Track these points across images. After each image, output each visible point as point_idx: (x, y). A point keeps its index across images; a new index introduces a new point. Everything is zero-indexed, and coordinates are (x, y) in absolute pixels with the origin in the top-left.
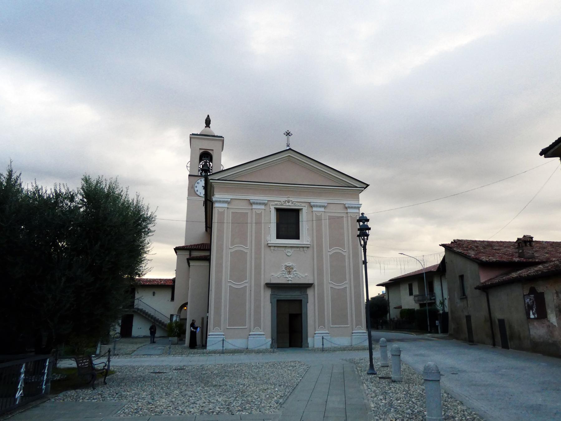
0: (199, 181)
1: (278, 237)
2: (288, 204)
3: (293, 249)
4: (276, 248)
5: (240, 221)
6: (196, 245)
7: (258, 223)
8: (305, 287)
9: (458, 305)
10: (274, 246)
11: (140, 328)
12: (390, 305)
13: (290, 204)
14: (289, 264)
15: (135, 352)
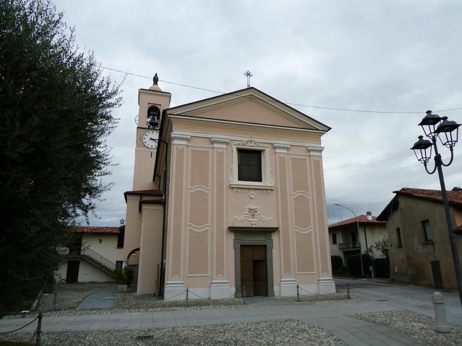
0: (147, 133)
1: (240, 179)
2: (250, 144)
5: (200, 158)
6: (147, 191)
8: (269, 232)
9: (419, 251)
10: (237, 188)
11: (85, 274)
13: (252, 144)
14: (252, 208)
15: (80, 305)
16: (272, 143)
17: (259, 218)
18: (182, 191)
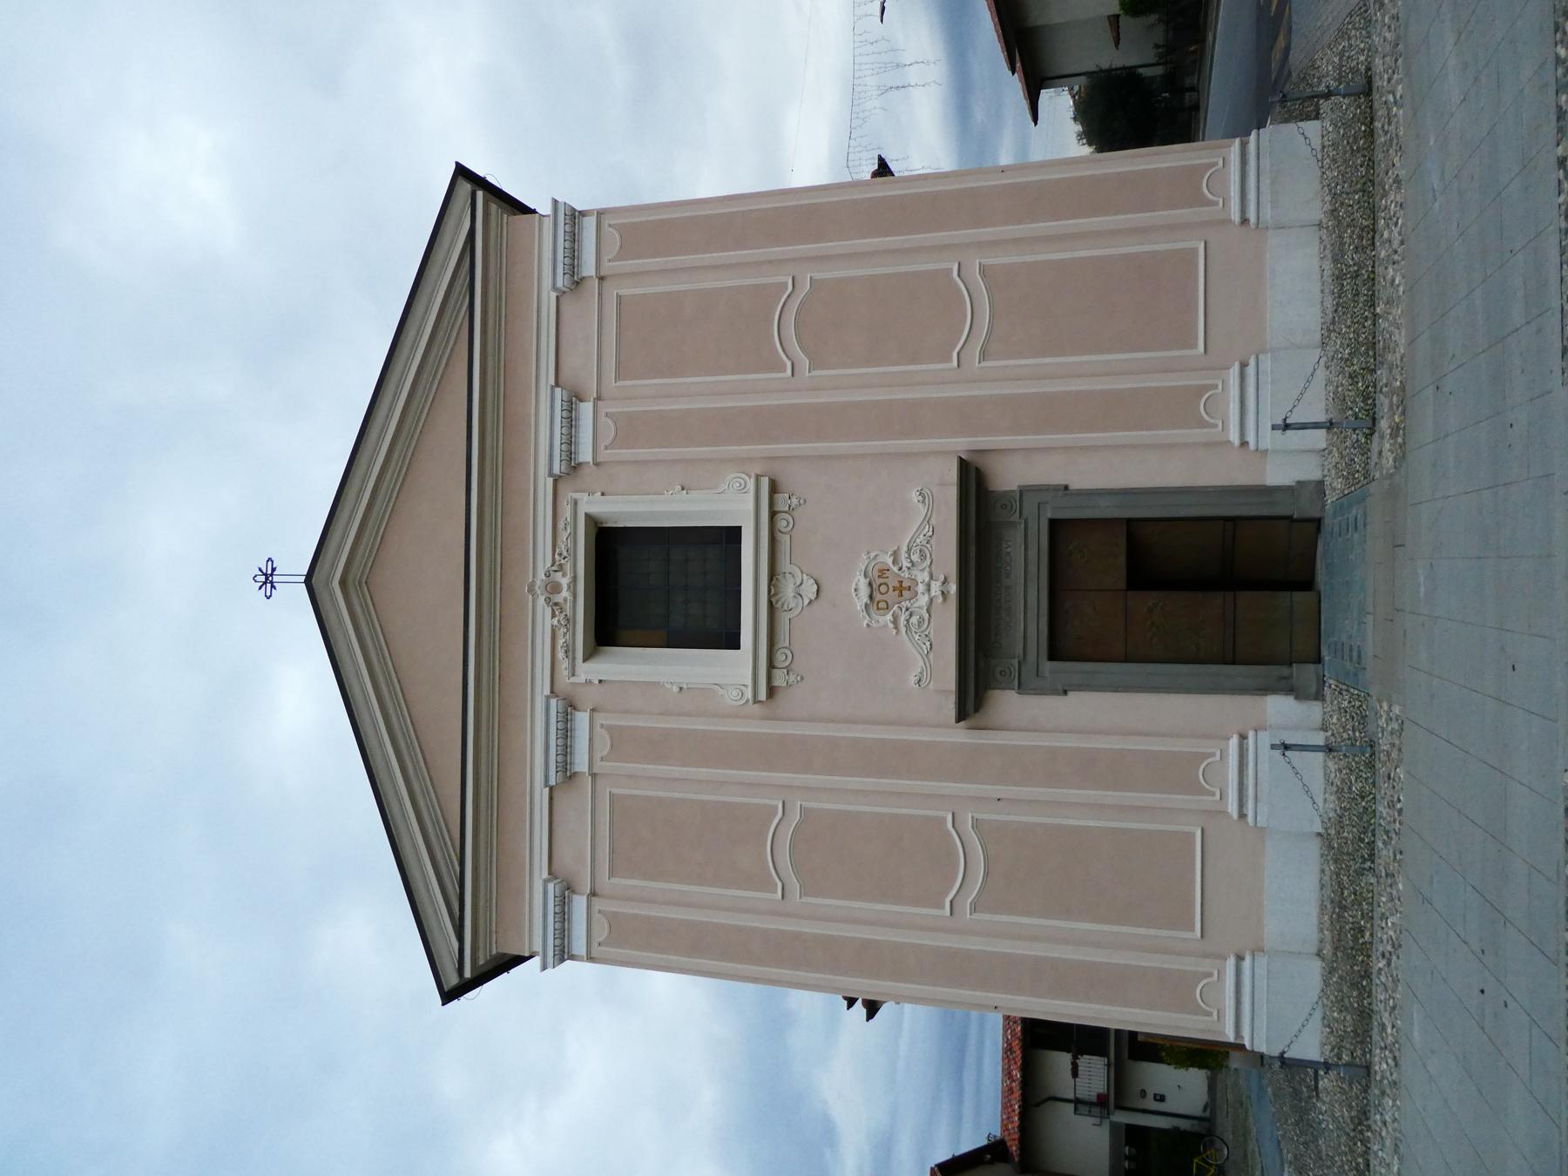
1: (733, 643)
2: (565, 593)
3: (785, 565)
4: (780, 658)
7: (656, 746)
8: (979, 503)
10: (771, 665)
12: (1105, 66)
13: (565, 582)
16: (550, 481)
17: (915, 558)
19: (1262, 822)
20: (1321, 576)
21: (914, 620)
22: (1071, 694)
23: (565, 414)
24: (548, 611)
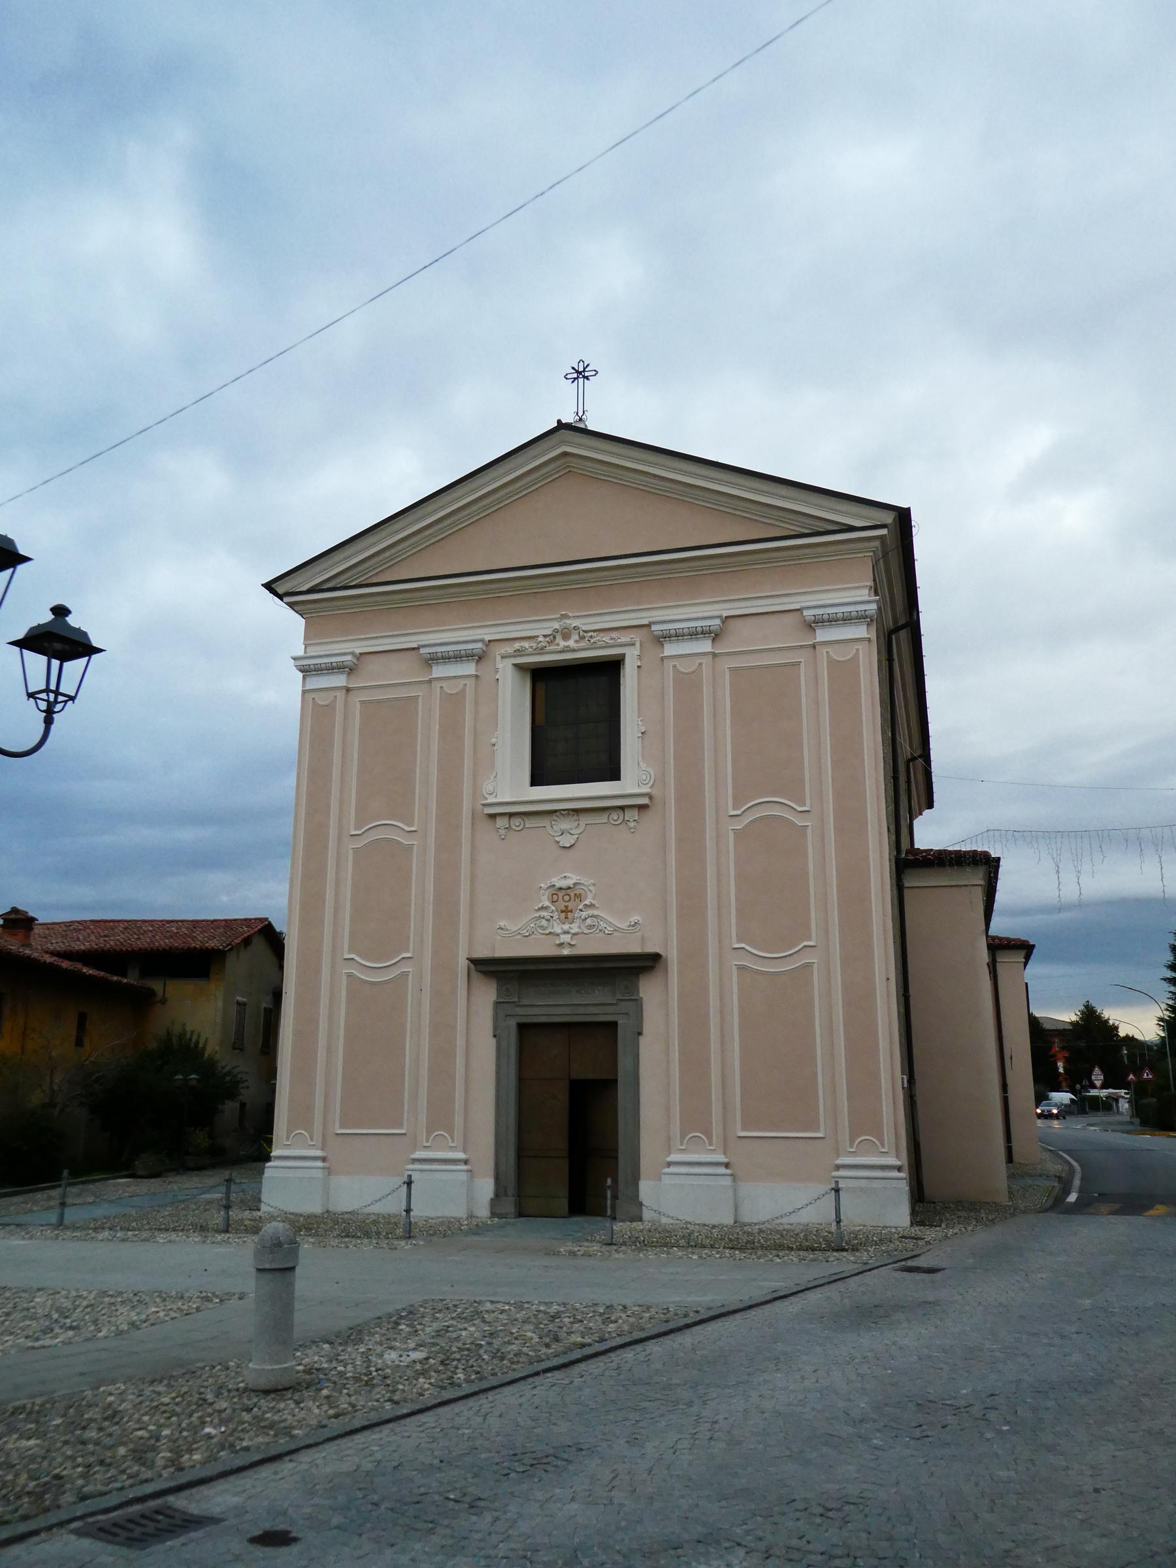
1: (537, 779)
2: (563, 644)
4: (516, 821)
7: (451, 729)
10: (511, 815)
13: (571, 643)
16: (646, 622)
17: (589, 921)
18: (326, 848)
19: (666, 1180)
20: (575, 1219)
21: (544, 923)
22: (493, 1041)
23: (699, 629)
24: (549, 632)
